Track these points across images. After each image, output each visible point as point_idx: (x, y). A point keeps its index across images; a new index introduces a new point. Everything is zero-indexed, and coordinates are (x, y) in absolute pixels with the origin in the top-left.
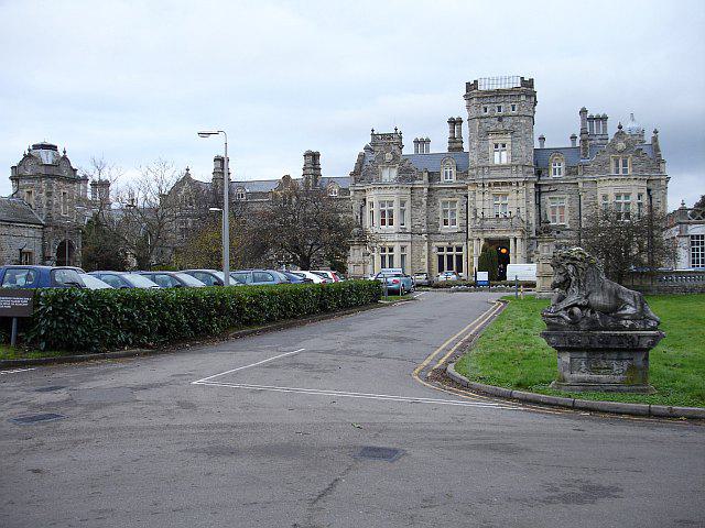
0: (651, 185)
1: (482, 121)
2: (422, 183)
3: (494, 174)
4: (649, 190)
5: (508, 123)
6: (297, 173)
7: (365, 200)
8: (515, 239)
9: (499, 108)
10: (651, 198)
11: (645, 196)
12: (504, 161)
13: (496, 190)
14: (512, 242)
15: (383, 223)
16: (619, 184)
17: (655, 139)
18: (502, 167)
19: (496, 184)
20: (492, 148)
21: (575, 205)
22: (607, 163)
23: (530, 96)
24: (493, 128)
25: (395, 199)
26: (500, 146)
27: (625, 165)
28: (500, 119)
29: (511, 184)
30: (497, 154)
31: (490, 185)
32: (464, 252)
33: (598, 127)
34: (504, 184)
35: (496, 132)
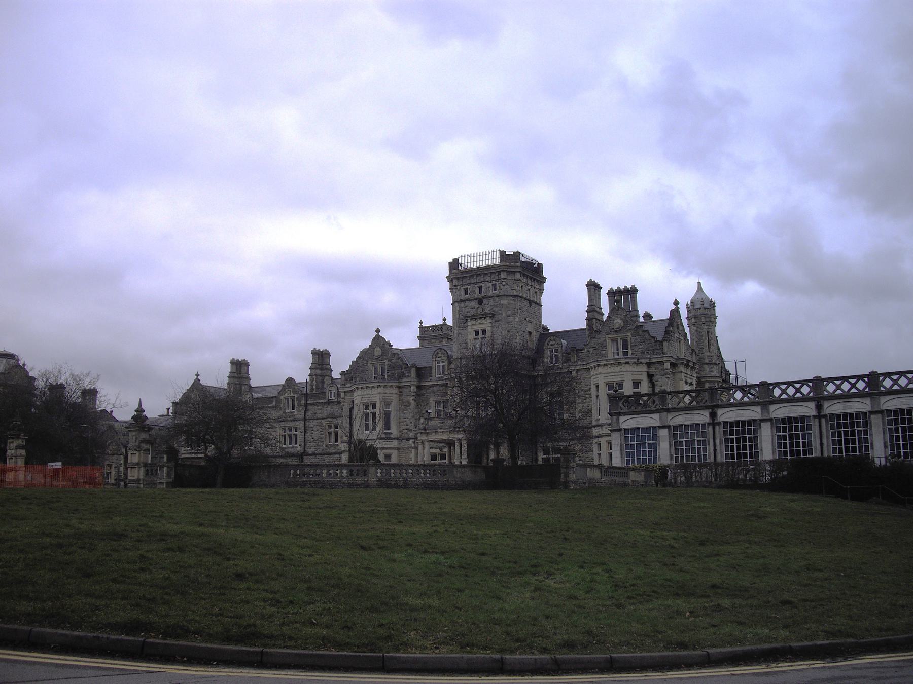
0: (653, 370)
1: (462, 305)
2: (410, 381)
4: (650, 377)
5: (488, 306)
6: (302, 375)
7: (353, 402)
9: (480, 288)
14: (457, 444)
22: (604, 345)
24: (472, 312)
26: (481, 333)
28: (480, 302)
33: (626, 301)
35: (475, 317)
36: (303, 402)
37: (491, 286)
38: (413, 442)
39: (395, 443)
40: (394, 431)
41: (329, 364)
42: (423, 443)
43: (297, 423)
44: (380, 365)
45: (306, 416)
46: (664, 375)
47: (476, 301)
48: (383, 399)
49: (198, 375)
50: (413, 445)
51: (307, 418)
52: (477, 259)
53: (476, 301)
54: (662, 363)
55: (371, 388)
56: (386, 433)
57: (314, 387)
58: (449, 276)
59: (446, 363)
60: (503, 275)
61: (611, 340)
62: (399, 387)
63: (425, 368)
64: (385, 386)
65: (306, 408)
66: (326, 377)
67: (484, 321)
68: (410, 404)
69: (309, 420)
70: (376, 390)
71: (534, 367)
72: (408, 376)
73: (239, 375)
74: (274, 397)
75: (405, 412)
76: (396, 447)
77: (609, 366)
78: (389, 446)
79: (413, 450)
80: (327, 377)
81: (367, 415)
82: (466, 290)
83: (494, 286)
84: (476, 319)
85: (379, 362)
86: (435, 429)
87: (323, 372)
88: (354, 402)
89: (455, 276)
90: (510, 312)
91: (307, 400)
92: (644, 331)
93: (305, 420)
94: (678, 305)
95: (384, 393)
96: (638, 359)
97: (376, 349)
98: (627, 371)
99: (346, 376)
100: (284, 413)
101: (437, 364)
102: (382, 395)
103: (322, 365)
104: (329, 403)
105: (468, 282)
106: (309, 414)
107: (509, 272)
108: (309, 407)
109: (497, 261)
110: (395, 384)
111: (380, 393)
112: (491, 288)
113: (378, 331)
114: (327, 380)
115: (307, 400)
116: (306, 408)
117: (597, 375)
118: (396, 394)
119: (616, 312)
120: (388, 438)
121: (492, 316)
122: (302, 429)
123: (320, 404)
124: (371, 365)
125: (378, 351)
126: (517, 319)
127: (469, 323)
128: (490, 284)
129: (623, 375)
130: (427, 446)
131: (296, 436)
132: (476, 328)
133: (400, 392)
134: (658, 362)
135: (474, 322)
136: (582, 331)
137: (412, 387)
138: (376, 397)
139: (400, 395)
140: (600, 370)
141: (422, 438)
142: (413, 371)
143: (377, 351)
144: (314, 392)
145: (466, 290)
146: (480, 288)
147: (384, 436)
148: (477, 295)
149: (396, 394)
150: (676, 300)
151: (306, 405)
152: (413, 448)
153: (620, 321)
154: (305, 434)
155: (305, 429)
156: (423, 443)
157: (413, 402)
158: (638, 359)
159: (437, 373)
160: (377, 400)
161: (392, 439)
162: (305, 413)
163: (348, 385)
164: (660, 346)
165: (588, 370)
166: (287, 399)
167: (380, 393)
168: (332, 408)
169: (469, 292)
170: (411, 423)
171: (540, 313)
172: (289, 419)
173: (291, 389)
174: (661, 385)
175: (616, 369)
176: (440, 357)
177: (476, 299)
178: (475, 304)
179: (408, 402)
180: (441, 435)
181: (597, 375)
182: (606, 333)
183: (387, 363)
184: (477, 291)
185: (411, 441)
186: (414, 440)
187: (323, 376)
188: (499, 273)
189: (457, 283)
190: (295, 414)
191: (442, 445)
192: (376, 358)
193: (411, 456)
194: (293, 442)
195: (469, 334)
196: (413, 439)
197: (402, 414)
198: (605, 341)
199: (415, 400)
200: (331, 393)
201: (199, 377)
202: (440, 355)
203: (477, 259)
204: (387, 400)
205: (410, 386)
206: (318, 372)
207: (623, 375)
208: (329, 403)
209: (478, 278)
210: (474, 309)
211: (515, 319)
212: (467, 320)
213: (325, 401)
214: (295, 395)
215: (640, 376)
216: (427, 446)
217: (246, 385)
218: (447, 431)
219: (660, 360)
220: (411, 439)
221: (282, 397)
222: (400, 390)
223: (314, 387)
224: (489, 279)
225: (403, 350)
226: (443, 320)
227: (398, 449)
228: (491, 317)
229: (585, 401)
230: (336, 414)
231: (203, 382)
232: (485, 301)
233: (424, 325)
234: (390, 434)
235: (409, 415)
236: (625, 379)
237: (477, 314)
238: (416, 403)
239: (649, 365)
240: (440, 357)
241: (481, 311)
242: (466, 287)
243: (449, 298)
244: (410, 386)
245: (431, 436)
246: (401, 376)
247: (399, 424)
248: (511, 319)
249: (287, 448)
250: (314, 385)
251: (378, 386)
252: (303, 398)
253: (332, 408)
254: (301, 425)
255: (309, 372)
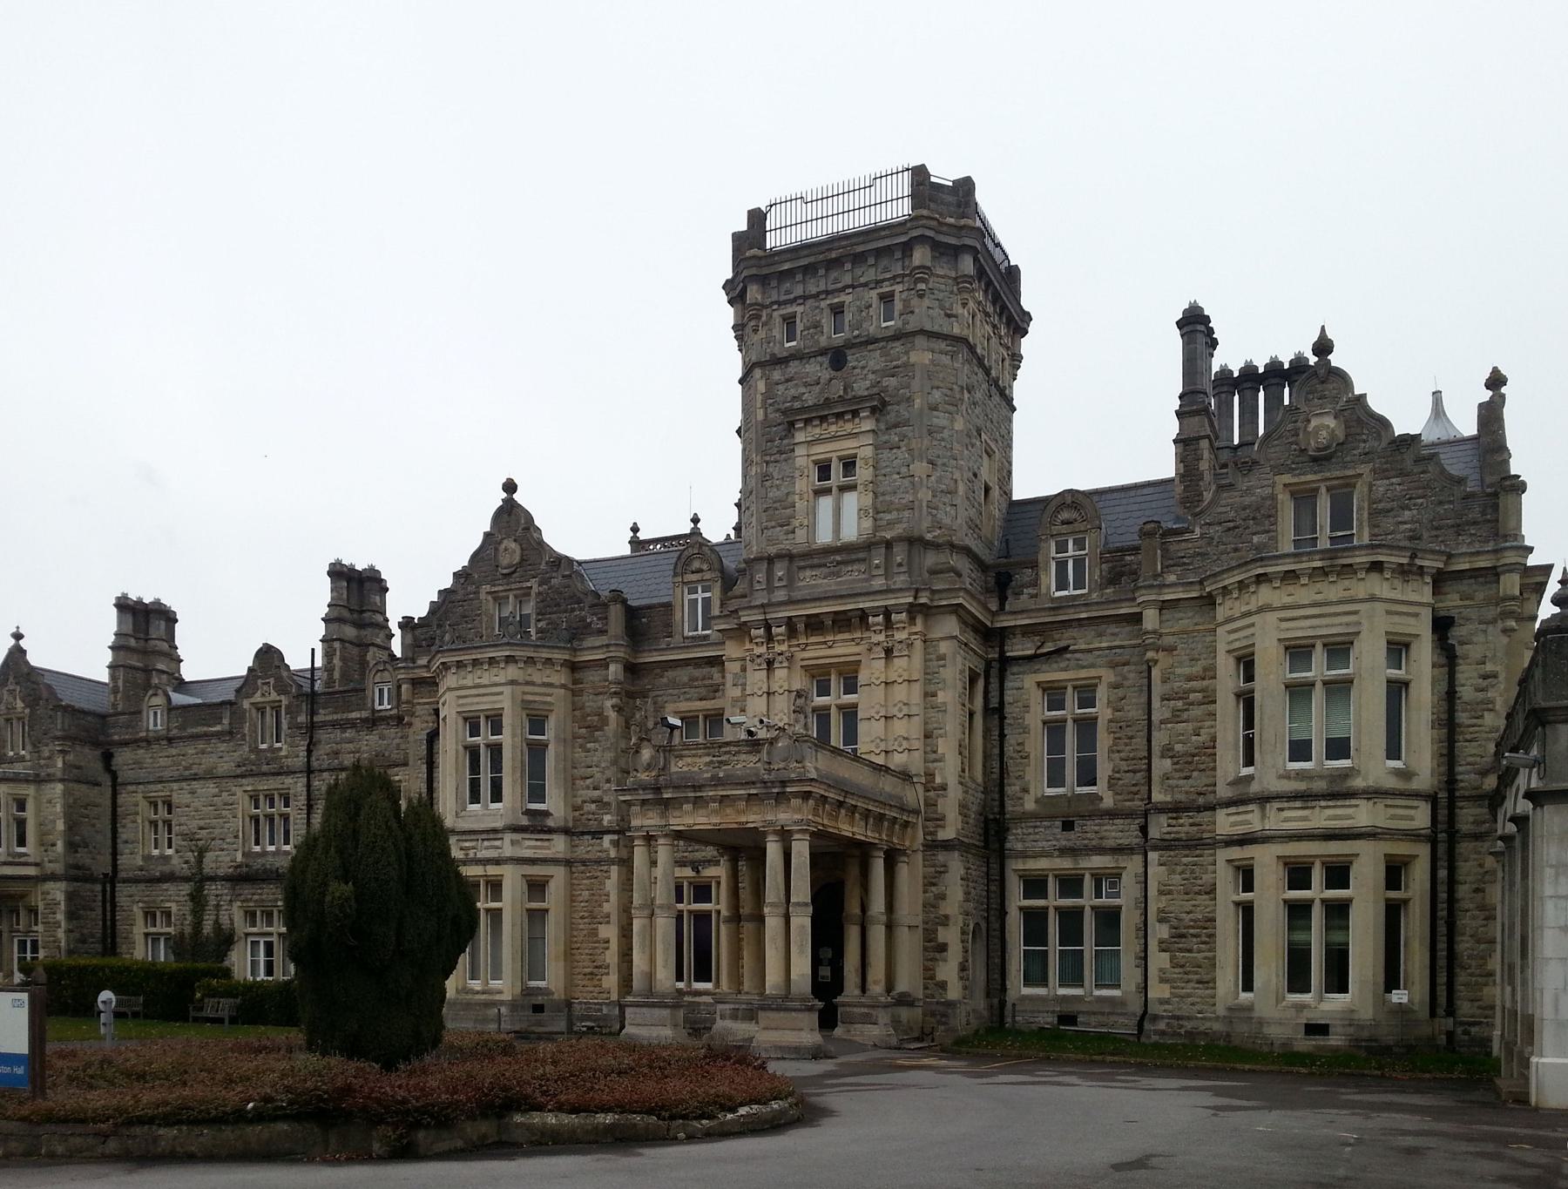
0: (1451, 601)
1: (777, 375)
3: (811, 581)
4: (1442, 626)
5: (865, 371)
7: (437, 712)
8: (785, 836)
10: (1448, 655)
11: (1424, 653)
12: (851, 531)
13: (817, 651)
14: (773, 850)
15: (1298, 978)
16: (1303, 594)
17: (1491, 415)
18: (842, 554)
19: (815, 625)
20: (806, 482)
21: (1134, 712)
22: (1264, 515)
23: (955, 252)
25: (505, 702)
26: (836, 470)
27: (1341, 518)
28: (837, 358)
29: (863, 615)
30: (826, 503)
31: (792, 632)
32: (29, 814)
34: (842, 622)
35: (823, 413)
36: (302, 718)
37: (875, 301)
38: (612, 842)
39: (558, 846)
40: (555, 804)
41: (383, 613)
42: (649, 839)
43: (289, 780)
44: (516, 597)
45: (313, 759)
46: (1493, 622)
47: (825, 360)
48: (523, 701)
49: (18, 636)
50: (613, 854)
51: (315, 764)
52: (829, 207)
53: (825, 360)
54: (1493, 574)
55: (486, 666)
56: (528, 812)
57: (337, 675)
58: (735, 276)
59: (715, 594)
60: (920, 256)
61: (1292, 494)
62: (574, 667)
63: (650, 607)
64: (530, 661)
65: (311, 738)
66: (371, 648)
67: (849, 427)
68: (604, 721)
69: (321, 771)
70: (502, 672)
71: (1003, 600)
72: (602, 632)
73: (142, 643)
74: (223, 703)
75: (589, 745)
76: (560, 856)
77: (1304, 580)
78: (541, 854)
79: (614, 869)
80: (376, 649)
81: (474, 752)
82: (789, 321)
83: (887, 299)
84: (823, 419)
85: (513, 586)
86: (695, 788)
87: (363, 633)
88: (438, 716)
89: (754, 271)
90: (937, 394)
91: (313, 713)
92: (1419, 460)
93: (309, 771)
94: (1503, 390)
95: (528, 683)
96: (1413, 556)
97: (503, 546)
98: (1373, 599)
99: (418, 632)
100: (255, 750)
101: (687, 597)
102: (519, 689)
103: (362, 612)
104: (374, 721)
105: (799, 291)
106: (321, 751)
107: (939, 249)
108: (321, 735)
109: (903, 209)
110: (558, 656)
111: (512, 682)
112: (877, 308)
113: (510, 487)
114: (372, 655)
115: (313, 713)
116: (311, 738)
117: (1248, 614)
118: (563, 686)
119: (1319, 387)
120: (536, 825)
121: (879, 409)
122: (303, 799)
123: (352, 724)
124: (490, 598)
125: (511, 552)
126: (959, 425)
127: (800, 437)
128: (874, 294)
129: (1355, 613)
130: (663, 853)
131: (286, 818)
132: (821, 451)
133: (575, 682)
134: (1475, 573)
135: (817, 430)
136: (1150, 490)
137: (612, 668)
138: (502, 693)
139: (574, 693)
140: (1265, 594)
141: (645, 820)
142: (616, 612)
143: (506, 550)
144: (337, 688)
145: (789, 321)
146: (838, 310)
147: (525, 821)
148: (830, 336)
149: (563, 686)
150: (1495, 371)
151: (312, 727)
152: (612, 862)
153: (1331, 422)
154: (309, 814)
155: (309, 798)
156: (649, 839)
157: (612, 715)
158: (1413, 556)
159: (686, 625)
160: (505, 702)
161: (551, 831)
162: (309, 752)
163: (423, 661)
164: (1483, 513)
165: (1209, 601)
166: (260, 709)
167: (512, 682)
168: (382, 737)
169: (799, 326)
170: (608, 781)
171: (1010, 432)
172: (265, 768)
173: (272, 681)
174: (1479, 656)
175: (1333, 590)
176: (699, 571)
177: (823, 352)
178: (817, 369)
179: (600, 714)
180: (715, 812)
181: (1248, 614)
182: (1279, 470)
183: (535, 589)
184: (827, 322)
185: (607, 839)
186: (616, 837)
187: (363, 646)
188: (907, 248)
189: (759, 297)
190: (283, 753)
191: (710, 852)
192: (505, 575)
193: (607, 889)
194: (280, 836)
195: (797, 474)
196: (614, 832)
197: (579, 754)
198: (1273, 497)
199: (619, 709)
200: (381, 691)
201: (21, 642)
202: (696, 565)
203: (829, 207)
204: (536, 706)
205: (604, 664)
206: (350, 632)
207: (1355, 613)
208: (374, 721)
209: (834, 275)
210: (817, 389)
211: (952, 421)
212: (792, 424)
213: (365, 714)
214: (283, 697)
215: (1412, 621)
216: (663, 853)
217: (163, 672)
218: (739, 797)
219: (1483, 563)
220: (608, 832)
221: (246, 704)
222: (577, 676)
223: (337, 675)
224: (870, 275)
225: (586, 562)
226: (692, 520)
227: (568, 863)
228: (873, 410)
229: (1185, 716)
230: (394, 756)
231: (36, 659)
232: (852, 359)
233: (642, 536)
234: (546, 814)
235: (601, 757)
236: (1365, 628)
237: (828, 403)
238: (622, 719)
239: (1440, 580)
240: (699, 571)
241: (841, 393)
242: (789, 310)
243: (732, 362)
244: (604, 664)
245: (677, 813)
246: (578, 632)
247: (571, 783)
248: (940, 419)
249: (264, 853)
250: (337, 668)
251: (510, 659)
252: (304, 707)
253: (382, 737)
254: (297, 785)
255: (321, 630)
